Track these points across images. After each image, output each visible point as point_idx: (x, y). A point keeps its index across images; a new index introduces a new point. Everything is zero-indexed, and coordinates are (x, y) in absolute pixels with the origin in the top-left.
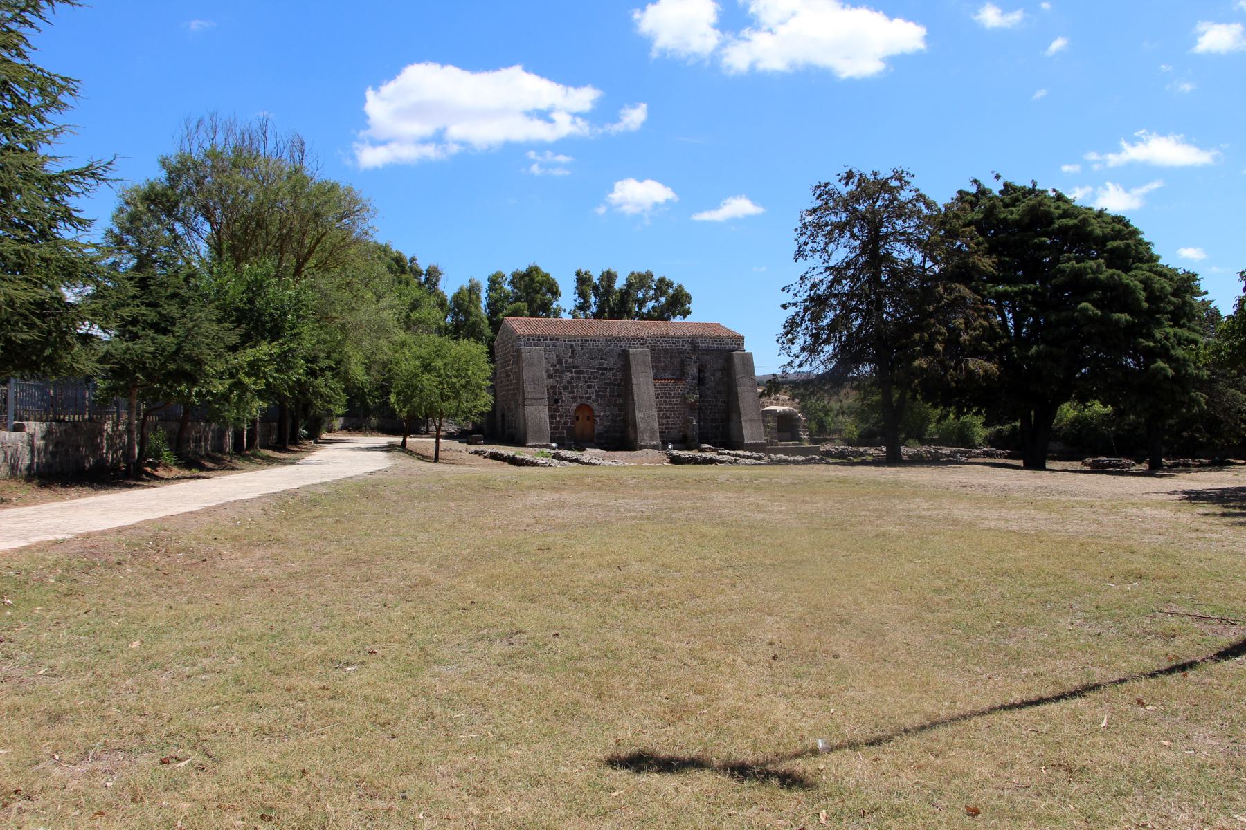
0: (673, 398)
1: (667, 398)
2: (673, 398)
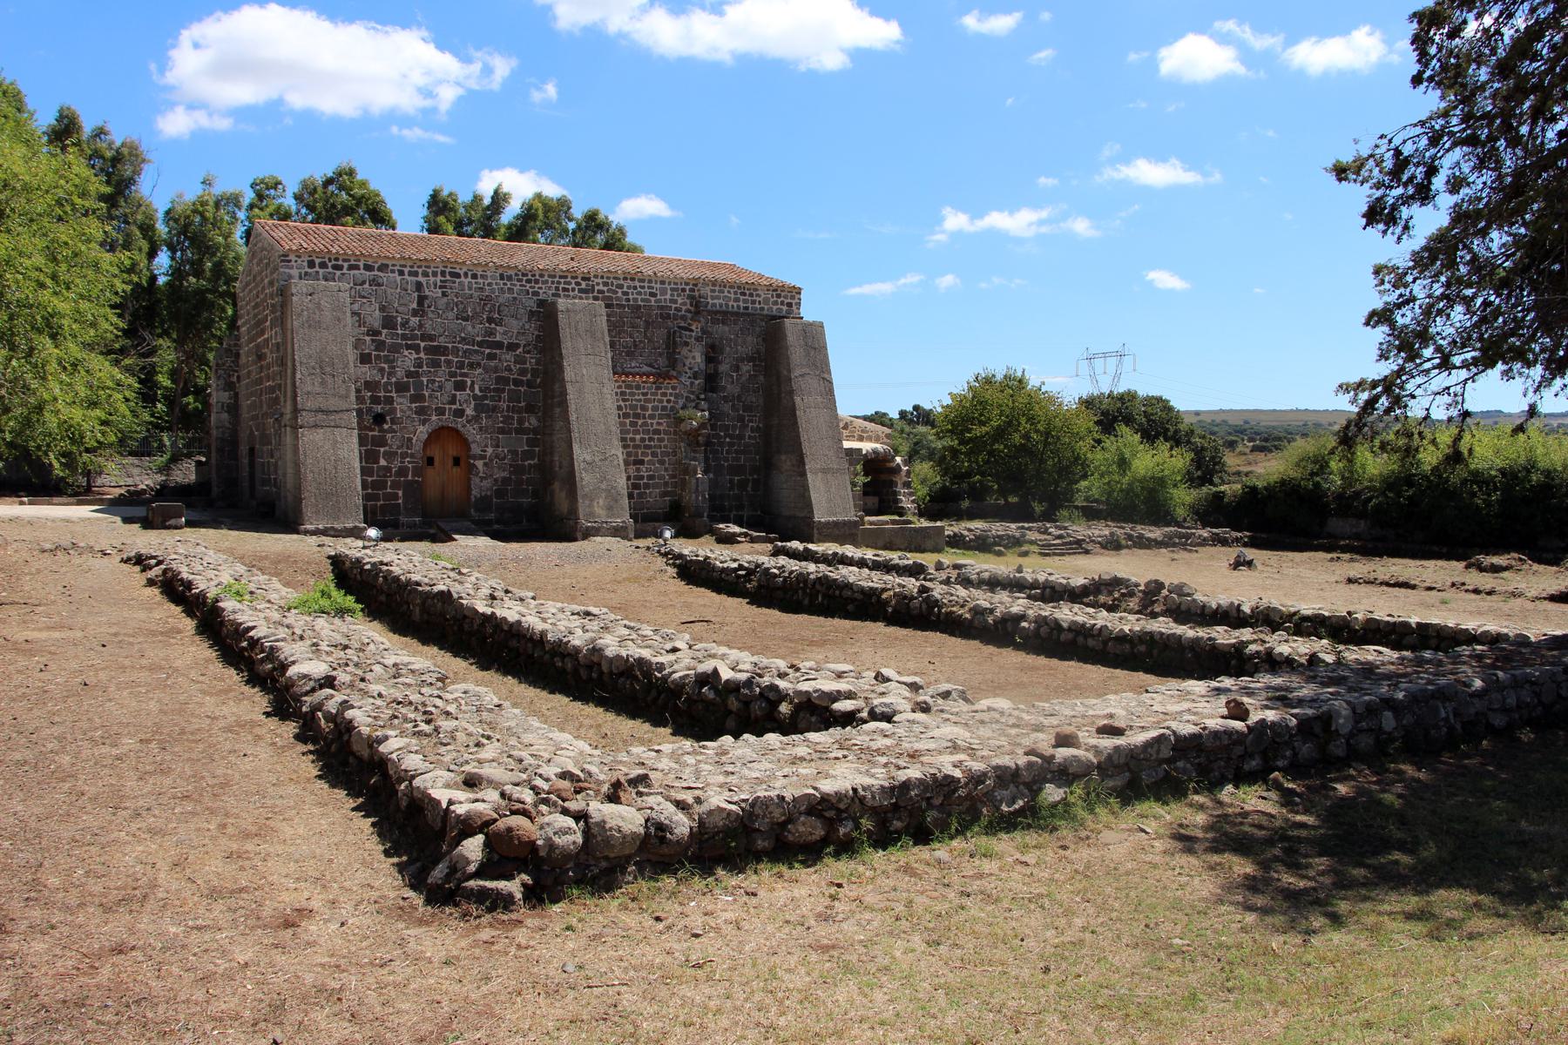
1: (637, 416)
2: (652, 417)
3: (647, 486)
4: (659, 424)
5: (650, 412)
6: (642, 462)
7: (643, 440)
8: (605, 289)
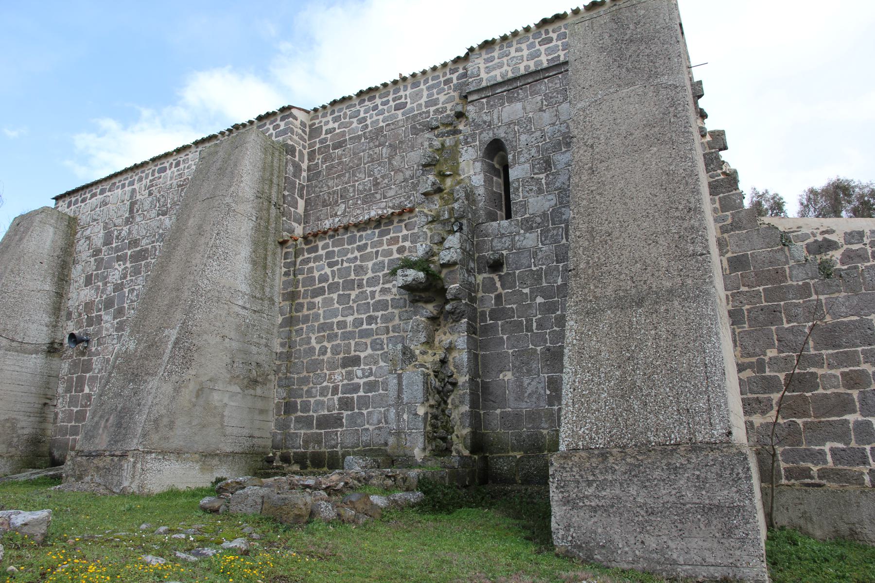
0: (372, 282)
1: (349, 285)
2: (372, 282)
3: (364, 402)
4: (384, 291)
5: (370, 274)
6: (355, 361)
7: (358, 323)
8: (336, 125)
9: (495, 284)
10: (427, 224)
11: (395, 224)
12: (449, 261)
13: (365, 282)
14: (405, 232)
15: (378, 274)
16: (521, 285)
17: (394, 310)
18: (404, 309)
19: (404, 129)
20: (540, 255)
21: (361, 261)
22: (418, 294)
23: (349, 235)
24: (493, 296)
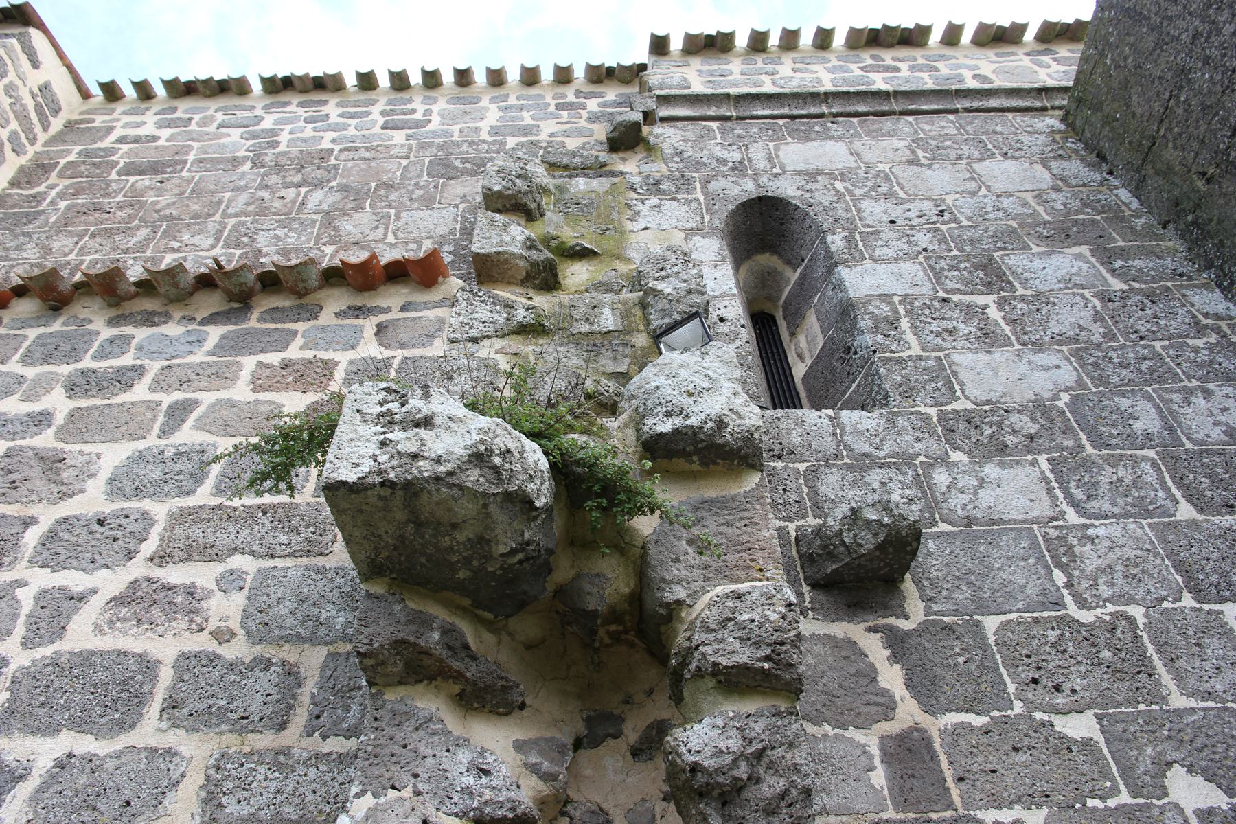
9: (871, 675)
10: (501, 334)
11: (327, 317)
12: (720, 424)
13: (31, 537)
14: (370, 349)
15: (147, 504)
16: (1039, 695)
17: (177, 739)
18: (266, 740)
19: (405, 162)
20: (1090, 559)
21: (61, 436)
22: (439, 612)
23: (57, 326)
24: (870, 740)
